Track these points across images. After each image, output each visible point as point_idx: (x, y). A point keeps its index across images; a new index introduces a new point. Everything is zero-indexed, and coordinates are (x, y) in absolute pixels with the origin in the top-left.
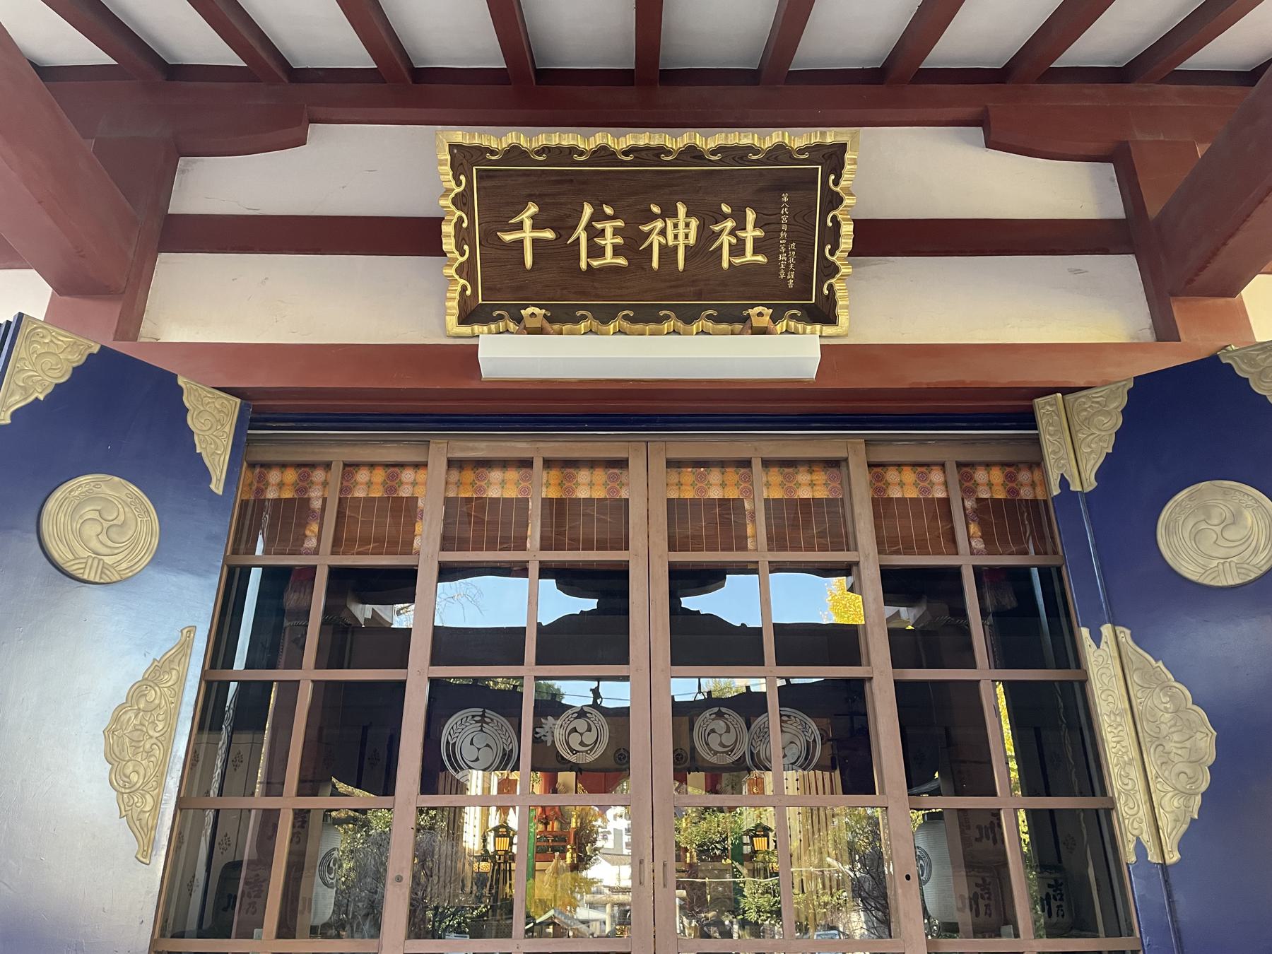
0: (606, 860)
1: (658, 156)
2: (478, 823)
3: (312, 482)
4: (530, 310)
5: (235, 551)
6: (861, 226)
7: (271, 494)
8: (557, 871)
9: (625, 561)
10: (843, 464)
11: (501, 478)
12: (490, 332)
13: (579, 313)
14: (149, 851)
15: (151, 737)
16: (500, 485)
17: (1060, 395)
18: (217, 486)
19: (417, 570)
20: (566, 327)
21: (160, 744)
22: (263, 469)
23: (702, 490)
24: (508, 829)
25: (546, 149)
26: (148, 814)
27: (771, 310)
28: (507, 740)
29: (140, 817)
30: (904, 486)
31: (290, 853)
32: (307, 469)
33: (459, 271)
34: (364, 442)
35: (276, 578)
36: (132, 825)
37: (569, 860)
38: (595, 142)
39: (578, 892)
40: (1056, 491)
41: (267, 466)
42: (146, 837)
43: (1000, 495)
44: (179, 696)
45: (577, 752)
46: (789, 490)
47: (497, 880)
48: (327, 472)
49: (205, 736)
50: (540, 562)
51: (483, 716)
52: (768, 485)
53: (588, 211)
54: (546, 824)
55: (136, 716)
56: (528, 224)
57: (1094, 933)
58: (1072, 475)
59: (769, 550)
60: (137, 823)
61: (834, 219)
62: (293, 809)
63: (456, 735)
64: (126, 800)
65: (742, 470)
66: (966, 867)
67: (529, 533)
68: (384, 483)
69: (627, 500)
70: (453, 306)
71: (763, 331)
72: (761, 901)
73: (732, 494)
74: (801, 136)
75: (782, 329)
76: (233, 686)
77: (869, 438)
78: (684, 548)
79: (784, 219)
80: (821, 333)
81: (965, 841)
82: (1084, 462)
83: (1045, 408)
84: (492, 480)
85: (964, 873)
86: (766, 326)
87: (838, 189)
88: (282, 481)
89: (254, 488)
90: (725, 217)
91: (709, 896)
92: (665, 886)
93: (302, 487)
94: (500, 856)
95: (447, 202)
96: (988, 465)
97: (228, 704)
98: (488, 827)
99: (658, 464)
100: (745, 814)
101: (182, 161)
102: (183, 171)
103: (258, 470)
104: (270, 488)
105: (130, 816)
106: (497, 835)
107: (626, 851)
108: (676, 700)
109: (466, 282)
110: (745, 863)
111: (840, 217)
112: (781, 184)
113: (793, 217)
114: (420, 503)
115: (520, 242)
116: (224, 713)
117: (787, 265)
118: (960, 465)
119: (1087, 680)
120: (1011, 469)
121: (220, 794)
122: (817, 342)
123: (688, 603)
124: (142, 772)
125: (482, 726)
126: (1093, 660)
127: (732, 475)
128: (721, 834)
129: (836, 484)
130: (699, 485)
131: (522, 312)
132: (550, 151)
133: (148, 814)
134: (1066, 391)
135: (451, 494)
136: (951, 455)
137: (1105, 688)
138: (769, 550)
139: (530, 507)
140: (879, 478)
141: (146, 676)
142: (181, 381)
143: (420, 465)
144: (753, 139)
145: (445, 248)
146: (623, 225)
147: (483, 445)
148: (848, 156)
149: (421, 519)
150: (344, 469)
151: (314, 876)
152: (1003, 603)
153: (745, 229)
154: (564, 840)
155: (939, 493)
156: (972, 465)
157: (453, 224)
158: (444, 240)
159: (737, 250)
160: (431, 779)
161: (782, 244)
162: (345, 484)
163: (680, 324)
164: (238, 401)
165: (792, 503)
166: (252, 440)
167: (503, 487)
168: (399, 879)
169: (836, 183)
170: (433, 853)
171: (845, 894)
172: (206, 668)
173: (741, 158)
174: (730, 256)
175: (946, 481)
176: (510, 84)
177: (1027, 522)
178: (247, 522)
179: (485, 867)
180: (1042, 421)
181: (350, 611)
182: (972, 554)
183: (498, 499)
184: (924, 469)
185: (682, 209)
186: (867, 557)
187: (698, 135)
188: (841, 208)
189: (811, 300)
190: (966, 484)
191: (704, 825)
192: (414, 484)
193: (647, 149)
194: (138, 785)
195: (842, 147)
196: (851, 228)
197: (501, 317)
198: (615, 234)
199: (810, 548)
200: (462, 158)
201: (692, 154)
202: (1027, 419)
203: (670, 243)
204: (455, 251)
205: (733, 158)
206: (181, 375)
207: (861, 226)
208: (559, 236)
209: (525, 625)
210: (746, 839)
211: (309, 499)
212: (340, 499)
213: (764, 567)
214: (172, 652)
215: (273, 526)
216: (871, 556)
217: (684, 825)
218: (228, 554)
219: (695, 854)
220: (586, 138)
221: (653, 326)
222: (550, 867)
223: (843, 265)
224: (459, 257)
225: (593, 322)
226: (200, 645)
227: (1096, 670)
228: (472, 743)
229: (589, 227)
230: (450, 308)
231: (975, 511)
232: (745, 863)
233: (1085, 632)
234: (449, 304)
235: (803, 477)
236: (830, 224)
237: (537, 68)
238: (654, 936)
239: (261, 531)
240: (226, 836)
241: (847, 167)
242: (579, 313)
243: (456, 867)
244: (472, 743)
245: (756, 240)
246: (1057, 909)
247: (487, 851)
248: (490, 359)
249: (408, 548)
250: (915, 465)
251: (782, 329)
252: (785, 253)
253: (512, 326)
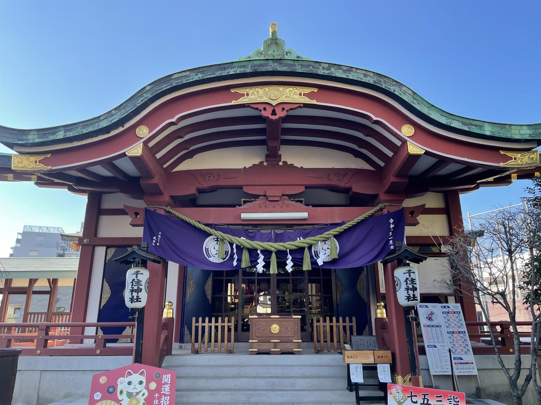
28: (226, 247)
63: (209, 245)
107: (269, 303)
168: (240, 306)
228: (214, 248)
244: (214, 248)
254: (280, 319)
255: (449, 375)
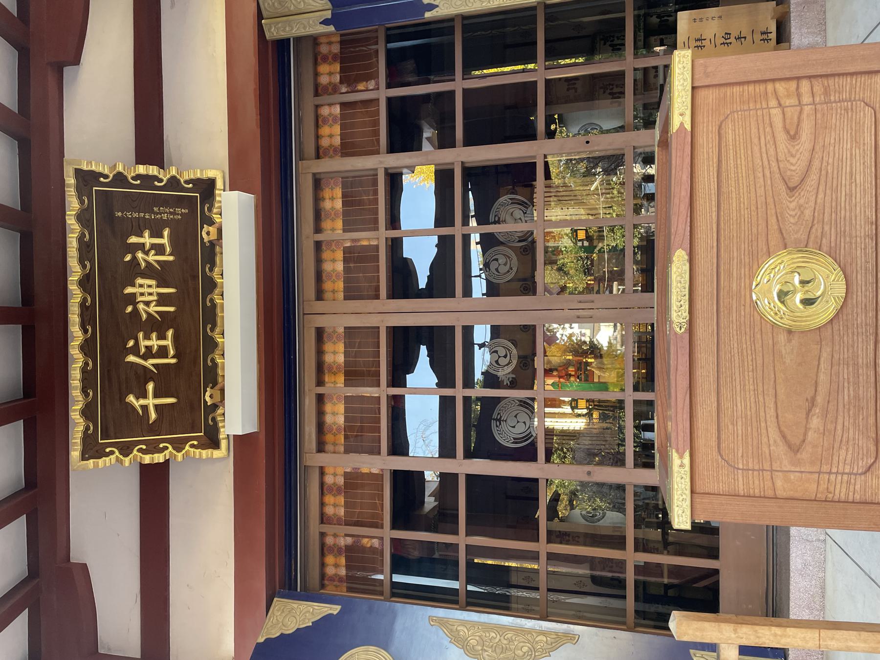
0: (597, 334)
1: (87, 308)
2: (569, 420)
3: (334, 545)
4: (208, 399)
5: (381, 593)
6: (141, 158)
7: (343, 572)
8: (600, 369)
9: (387, 329)
10: (318, 176)
11: (331, 415)
12: (224, 427)
13: (210, 364)
14: (571, 635)
15: (500, 640)
16: (336, 415)
17: (263, 21)
18: (335, 609)
19: (394, 470)
20: (220, 372)
21: (505, 634)
22: (326, 579)
23: (337, 276)
24: (571, 401)
25: (84, 390)
26: (548, 638)
27: (205, 225)
28: (502, 410)
29: (549, 643)
30: (332, 135)
31: (585, 545)
32: (325, 549)
33: (179, 450)
34: (305, 510)
35: (400, 564)
36: (555, 648)
37: (593, 360)
38: (78, 354)
39: (616, 352)
40: (331, 28)
41: (323, 576)
42: (561, 639)
43: (337, 67)
44: (474, 624)
45: (510, 360)
46: (336, 215)
47: (606, 406)
48: (327, 535)
49: (514, 606)
50: (387, 387)
51: (496, 420)
52: (333, 230)
53: (131, 358)
54: (570, 375)
55: (486, 651)
56: (142, 402)
57: (623, 20)
58: (321, 16)
59: (378, 230)
60: (553, 645)
61: (134, 178)
62: (547, 543)
64: (540, 653)
65: (324, 247)
66: (593, 100)
67: (369, 395)
68: (334, 495)
69: (345, 328)
70: (206, 453)
71: (220, 231)
72: (618, 234)
73: (340, 255)
74: (70, 202)
75: (219, 218)
76: (470, 588)
77: (298, 158)
78: (377, 289)
79: (136, 215)
80: (221, 190)
81: (576, 100)
82: (310, 7)
83: (274, 31)
84: (332, 421)
85: (597, 102)
86: (216, 230)
87: (111, 176)
88: (333, 565)
89: (338, 584)
90: (134, 258)
91: (615, 269)
92: (593, 302)
93: (337, 551)
94: (590, 405)
95: (127, 461)
96: (316, 74)
97: (483, 591)
98: (572, 414)
99: (319, 306)
100: (566, 245)
101: (101, 651)
102: (109, 649)
103: (326, 582)
104: (339, 573)
105: (549, 650)
106: (576, 407)
108: (485, 292)
109: (188, 444)
110: (594, 245)
111: (133, 174)
112: (107, 217)
113: (134, 209)
114: (348, 470)
115: (157, 407)
116: (489, 593)
117: (171, 213)
118: (316, 94)
119: (462, 15)
120: (319, 58)
121: (537, 589)
122: (228, 193)
123: (422, 283)
124: (522, 644)
125: (503, 421)
126: (446, 11)
127: (326, 255)
128: (578, 260)
129: (332, 181)
130: (334, 278)
131: (209, 404)
132: (86, 387)
133: (548, 638)
134: (260, 16)
135: (342, 449)
136: (309, 100)
137: (464, 3)
138: (378, 230)
139: (351, 395)
140: (326, 154)
141: (461, 646)
142: (261, 640)
143: (322, 471)
144: (73, 237)
145: (162, 461)
146: (142, 333)
147: (307, 429)
148: (85, 167)
149: (359, 469)
150: (325, 523)
151: (599, 526)
152: (412, 69)
153: (144, 244)
154: (580, 363)
155: (337, 110)
156: (316, 86)
157: (143, 456)
158: (156, 461)
159: (159, 249)
160: (527, 453)
161: (154, 217)
162: (335, 522)
163: (217, 291)
164: (275, 599)
165: (345, 214)
166: (305, 588)
167: (337, 414)
168: (589, 473)
169: (106, 177)
170: (588, 449)
171: (614, 179)
172: (458, 607)
173: (88, 246)
174: (164, 255)
175: (328, 105)
176: (36, 417)
177: (357, 49)
178: (362, 587)
179: (596, 415)
180: (283, 35)
181: (427, 513)
182: (378, 89)
183: (346, 417)
184: (320, 120)
185: (129, 290)
186: (381, 162)
187: (70, 278)
188: (126, 174)
189: (197, 196)
190: (330, 90)
191: (572, 272)
192: (335, 475)
193: (82, 315)
194: (530, 646)
195: (79, 173)
196: (141, 167)
197: (214, 419)
198: (149, 339)
199: (376, 201)
200: (91, 450)
201: (85, 283)
202: (282, 45)
203: (155, 298)
204: (164, 454)
205: (88, 252)
206: (257, 640)
207: (141, 158)
208: (151, 379)
209: (438, 396)
210: (580, 244)
211: (346, 546)
212: (345, 525)
213: (394, 234)
214: (446, 631)
215: (364, 569)
216: (381, 160)
217: (571, 285)
218: (383, 598)
219: (589, 278)
220: (75, 361)
221: (218, 310)
222: (597, 372)
223: (169, 173)
224: (169, 451)
225: (216, 353)
226: (441, 612)
227: (452, 9)
228: (514, 427)
229: (145, 357)
230: (207, 456)
231: (349, 85)
232: (594, 245)
233: (428, 15)
234: (204, 456)
235: (327, 205)
236: (139, 182)
237: (22, 397)
238: (597, 309)
239: (369, 577)
240: (575, 584)
241: (94, 168)
242: (210, 364)
243: (597, 434)
244: (514, 427)
245: (152, 236)
246: (620, 40)
247: (586, 414)
248: (243, 426)
249: (379, 477)
250: (317, 126)
251: (219, 218)
252: (161, 215)
253: (220, 411)
254: (700, 442)
255: (550, 608)
